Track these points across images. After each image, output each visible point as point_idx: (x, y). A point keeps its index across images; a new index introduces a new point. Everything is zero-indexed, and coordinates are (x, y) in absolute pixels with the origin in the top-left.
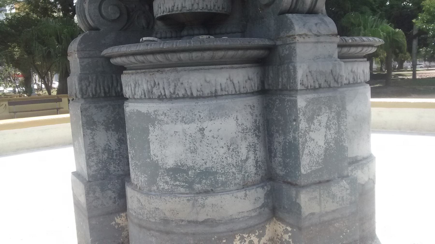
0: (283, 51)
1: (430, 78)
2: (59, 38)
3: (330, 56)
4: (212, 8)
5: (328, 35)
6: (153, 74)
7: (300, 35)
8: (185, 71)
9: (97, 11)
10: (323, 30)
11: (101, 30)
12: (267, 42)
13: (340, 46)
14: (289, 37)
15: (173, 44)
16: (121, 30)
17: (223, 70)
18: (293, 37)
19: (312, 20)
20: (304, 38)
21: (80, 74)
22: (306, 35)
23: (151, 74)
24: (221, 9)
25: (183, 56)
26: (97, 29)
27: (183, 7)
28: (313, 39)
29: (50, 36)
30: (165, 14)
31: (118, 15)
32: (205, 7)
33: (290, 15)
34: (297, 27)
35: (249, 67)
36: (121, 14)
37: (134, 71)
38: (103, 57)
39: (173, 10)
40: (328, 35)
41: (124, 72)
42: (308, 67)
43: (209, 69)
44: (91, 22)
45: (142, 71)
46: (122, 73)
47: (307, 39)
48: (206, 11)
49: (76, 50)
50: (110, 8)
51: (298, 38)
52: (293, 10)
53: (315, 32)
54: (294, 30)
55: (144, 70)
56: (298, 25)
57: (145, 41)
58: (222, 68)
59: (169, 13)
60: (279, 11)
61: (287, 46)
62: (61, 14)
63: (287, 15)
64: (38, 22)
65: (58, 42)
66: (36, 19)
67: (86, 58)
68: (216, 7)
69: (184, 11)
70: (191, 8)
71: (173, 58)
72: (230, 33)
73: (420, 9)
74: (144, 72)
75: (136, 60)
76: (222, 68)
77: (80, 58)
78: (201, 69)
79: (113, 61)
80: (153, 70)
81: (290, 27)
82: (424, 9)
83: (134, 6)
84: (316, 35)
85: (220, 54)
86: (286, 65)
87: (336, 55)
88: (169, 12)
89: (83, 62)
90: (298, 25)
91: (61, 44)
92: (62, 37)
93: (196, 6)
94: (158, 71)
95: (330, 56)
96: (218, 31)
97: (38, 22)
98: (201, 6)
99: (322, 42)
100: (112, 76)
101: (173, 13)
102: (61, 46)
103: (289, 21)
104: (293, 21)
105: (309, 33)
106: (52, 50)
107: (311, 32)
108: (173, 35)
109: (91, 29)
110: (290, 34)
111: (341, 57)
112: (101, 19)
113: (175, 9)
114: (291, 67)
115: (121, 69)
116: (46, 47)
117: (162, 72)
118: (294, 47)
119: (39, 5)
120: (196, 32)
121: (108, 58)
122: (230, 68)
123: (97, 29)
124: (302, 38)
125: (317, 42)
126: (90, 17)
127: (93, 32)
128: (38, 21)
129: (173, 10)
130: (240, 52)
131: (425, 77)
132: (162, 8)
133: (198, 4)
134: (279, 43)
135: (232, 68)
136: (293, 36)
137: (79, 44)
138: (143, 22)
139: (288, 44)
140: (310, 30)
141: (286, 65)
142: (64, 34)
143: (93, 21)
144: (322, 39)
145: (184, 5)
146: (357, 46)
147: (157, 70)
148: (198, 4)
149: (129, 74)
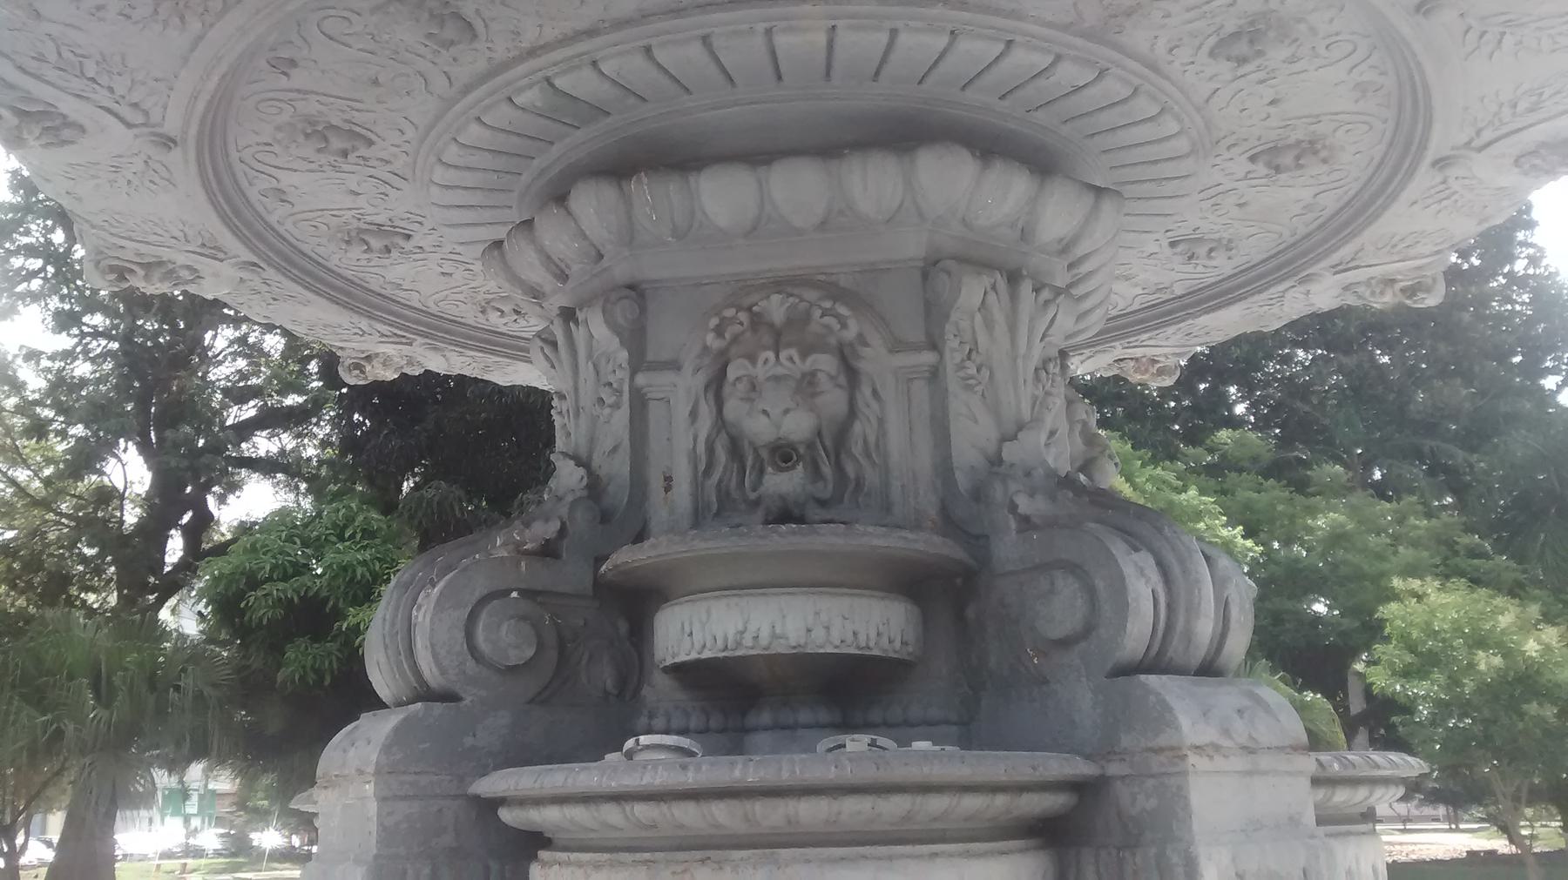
0: (1135, 800)
1: (1424, 862)
2: (103, 682)
3: (1294, 821)
4: (872, 644)
5: (1280, 749)
6: (685, 871)
7: (1198, 748)
8: (808, 861)
9: (460, 636)
10: (1265, 734)
11: (467, 702)
12: (1081, 768)
13: (1316, 782)
14: (1159, 750)
15: (780, 769)
16: (531, 701)
17: (938, 860)
18: (1176, 753)
19: (1226, 696)
20: (1211, 758)
21: (376, 857)
22: (1217, 748)
23: (679, 868)
24: (897, 644)
25: (810, 812)
26: (448, 697)
27: (774, 636)
28: (1239, 763)
29: (71, 677)
30: (707, 654)
31: (530, 652)
32: (850, 638)
33: (1152, 680)
34: (1185, 722)
35: (1021, 851)
36: (541, 647)
37: (606, 856)
38: (477, 800)
39: (739, 644)
40: (1280, 749)
41: (544, 854)
42: (1234, 860)
43: (890, 858)
44: (427, 674)
45: (638, 856)
46: (534, 857)
47: (1220, 763)
48: (853, 651)
49: (371, 769)
50: (504, 628)
51: (1193, 759)
52: (1156, 663)
53: (1243, 740)
54: (1178, 728)
55: (647, 856)
56: (1190, 713)
57: (647, 747)
58: (936, 855)
59: (721, 655)
60: (1109, 666)
61: (1150, 782)
62: (113, 599)
63: (1143, 677)
64: (27, 622)
65: (98, 697)
66: (22, 612)
67: (405, 798)
68: (885, 640)
69: (780, 648)
70: (802, 642)
71: (771, 814)
72: (918, 725)
73: (1373, 631)
74: (646, 862)
75: (627, 817)
76: (936, 855)
77: (382, 800)
78: (865, 857)
79: (506, 815)
80: (681, 856)
81: (1163, 717)
82: (1387, 630)
83: (581, 623)
84: (1244, 748)
85: (937, 804)
86: (1153, 851)
87: (1310, 817)
88: (726, 648)
89: (389, 814)
90: (1190, 713)
91: (108, 706)
92: (117, 680)
93: (819, 634)
94: (703, 861)
95: (1294, 821)
96: (875, 715)
97: (27, 622)
98: (836, 636)
99: (1265, 773)
100: (487, 868)
101: (739, 653)
102: (104, 714)
103: (1152, 698)
104: (1171, 700)
105: (1225, 743)
106: (70, 728)
107: (1231, 738)
108: (713, 724)
109: (425, 694)
110: (1162, 741)
111: (1325, 818)
112: (470, 664)
113: (748, 641)
114: (1175, 859)
115: (534, 842)
116: (49, 717)
117: (720, 865)
118: (1180, 788)
119: (41, 562)
120: (805, 716)
121: (491, 805)
122: (962, 855)
123: (448, 697)
124: (1206, 759)
125: (1249, 773)
126: (435, 655)
127: (438, 708)
128: (29, 619)
129: (739, 644)
130: (1001, 800)
131: (1403, 858)
132: (697, 637)
133: (827, 628)
134: (1114, 769)
135: (968, 855)
136: (1172, 749)
137: (387, 749)
138: (606, 676)
139: (1152, 776)
140: (1226, 732)
141: (1153, 851)
142: (126, 669)
143: (443, 672)
144: (1265, 761)
145: (778, 631)
146: (1354, 782)
147: (699, 855)
148: (827, 628)
149: (580, 865)
